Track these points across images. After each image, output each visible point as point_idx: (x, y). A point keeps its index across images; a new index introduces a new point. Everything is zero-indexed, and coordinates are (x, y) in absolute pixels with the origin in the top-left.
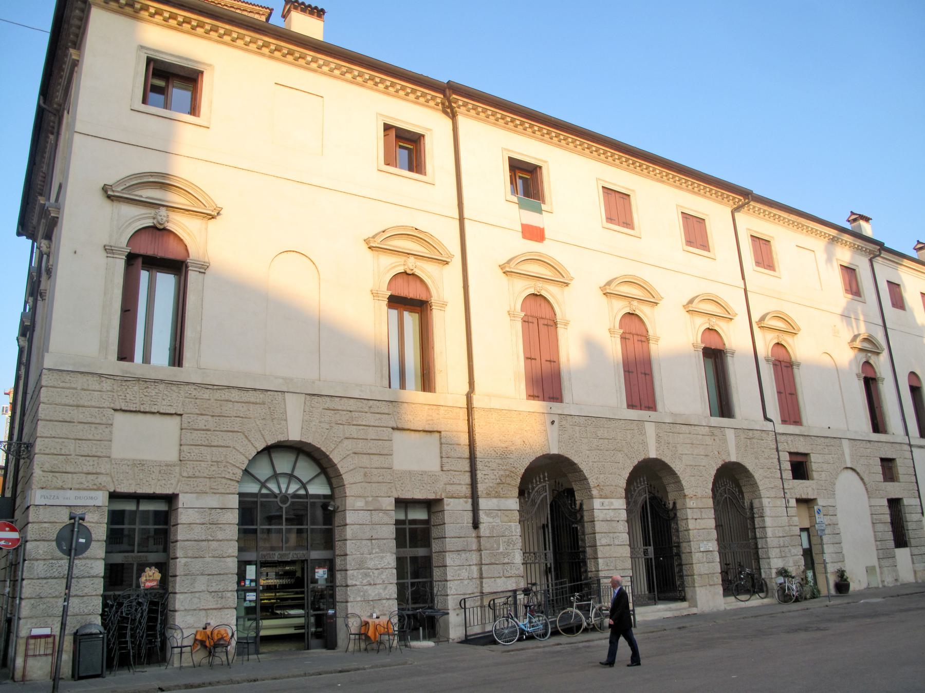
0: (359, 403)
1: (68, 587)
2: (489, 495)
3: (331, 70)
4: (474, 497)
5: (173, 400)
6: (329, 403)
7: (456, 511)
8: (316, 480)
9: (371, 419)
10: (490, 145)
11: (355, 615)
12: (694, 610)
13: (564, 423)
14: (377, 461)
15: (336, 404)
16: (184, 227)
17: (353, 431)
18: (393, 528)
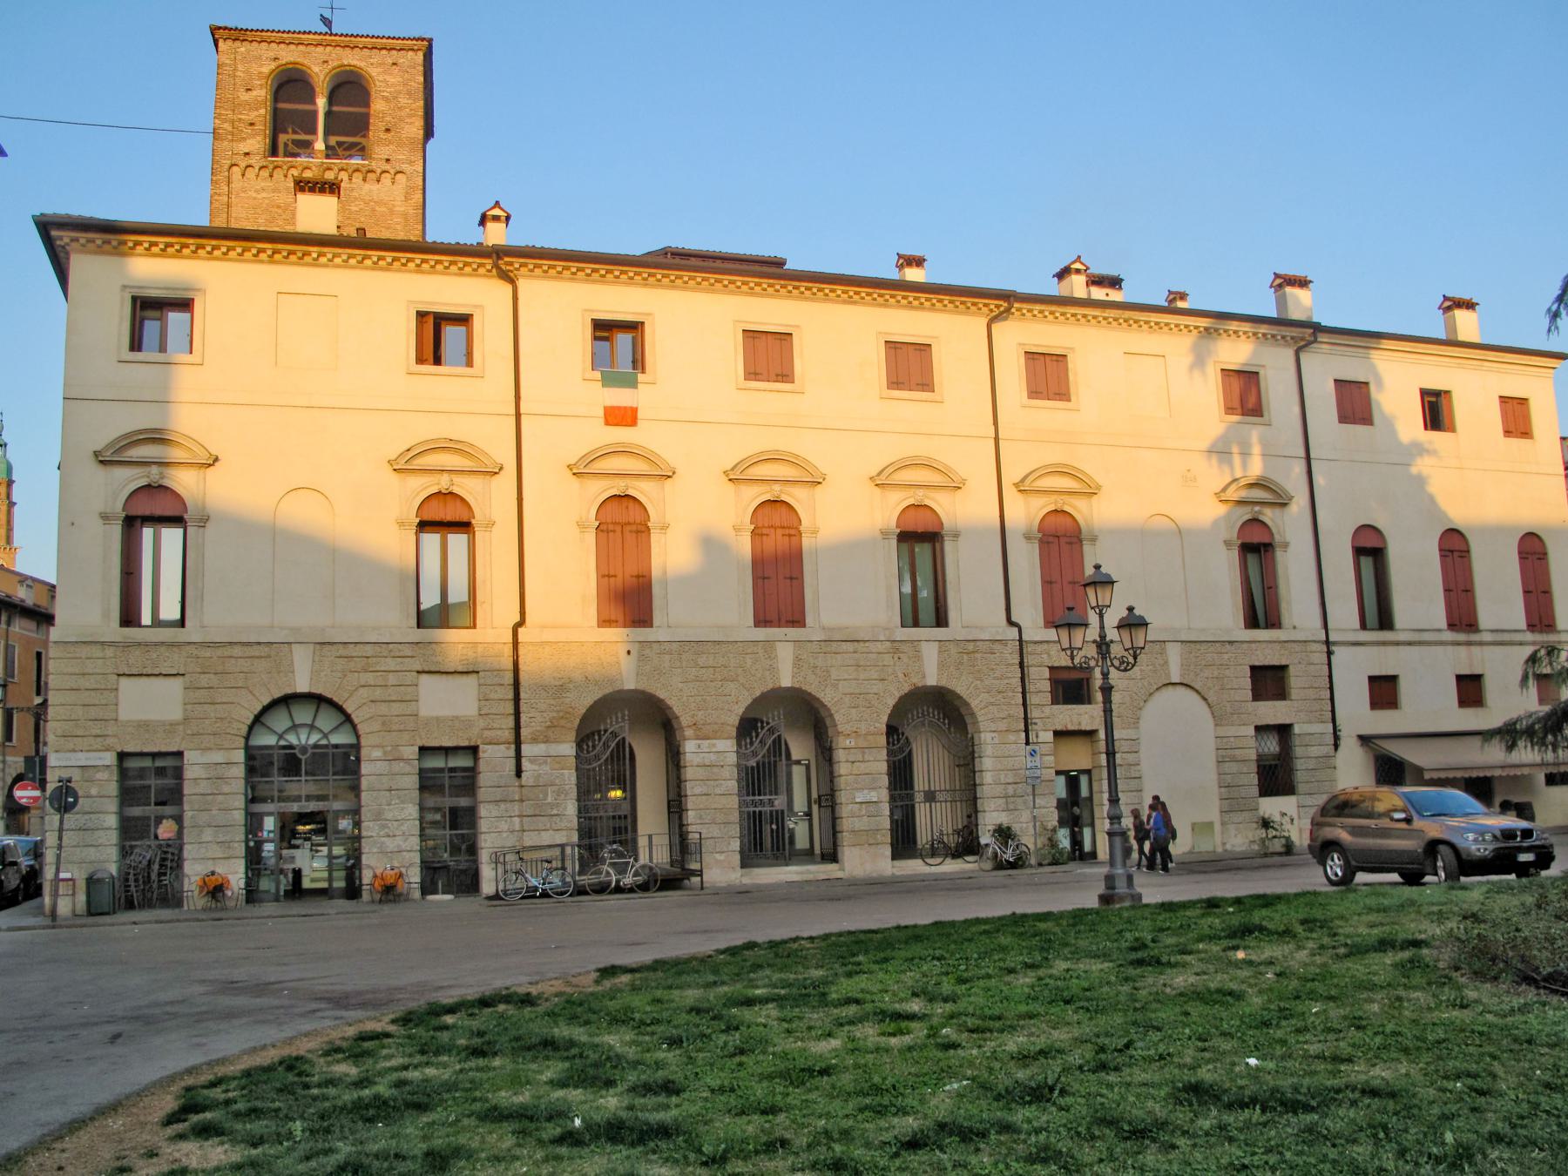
0: (377, 648)
1: (60, 838)
2: (535, 741)
3: (346, 261)
4: (518, 743)
5: (175, 661)
6: (342, 651)
7: (495, 758)
8: (341, 729)
9: (392, 664)
10: (560, 309)
11: (369, 867)
12: (840, 874)
13: (647, 651)
14: (397, 708)
15: (351, 651)
16: (184, 482)
17: (369, 678)
18: (416, 778)
